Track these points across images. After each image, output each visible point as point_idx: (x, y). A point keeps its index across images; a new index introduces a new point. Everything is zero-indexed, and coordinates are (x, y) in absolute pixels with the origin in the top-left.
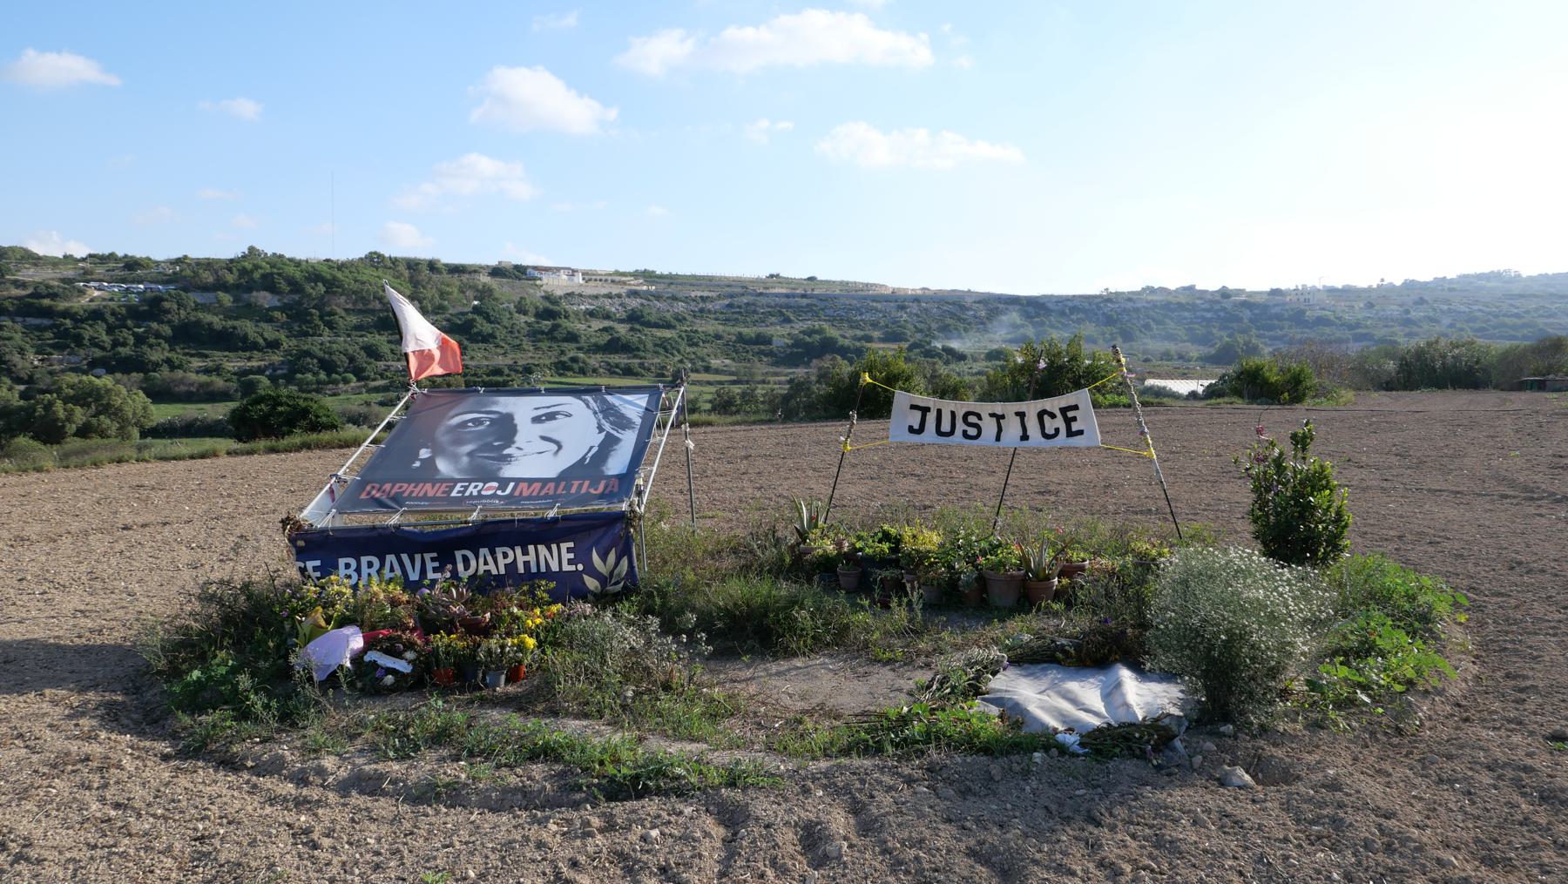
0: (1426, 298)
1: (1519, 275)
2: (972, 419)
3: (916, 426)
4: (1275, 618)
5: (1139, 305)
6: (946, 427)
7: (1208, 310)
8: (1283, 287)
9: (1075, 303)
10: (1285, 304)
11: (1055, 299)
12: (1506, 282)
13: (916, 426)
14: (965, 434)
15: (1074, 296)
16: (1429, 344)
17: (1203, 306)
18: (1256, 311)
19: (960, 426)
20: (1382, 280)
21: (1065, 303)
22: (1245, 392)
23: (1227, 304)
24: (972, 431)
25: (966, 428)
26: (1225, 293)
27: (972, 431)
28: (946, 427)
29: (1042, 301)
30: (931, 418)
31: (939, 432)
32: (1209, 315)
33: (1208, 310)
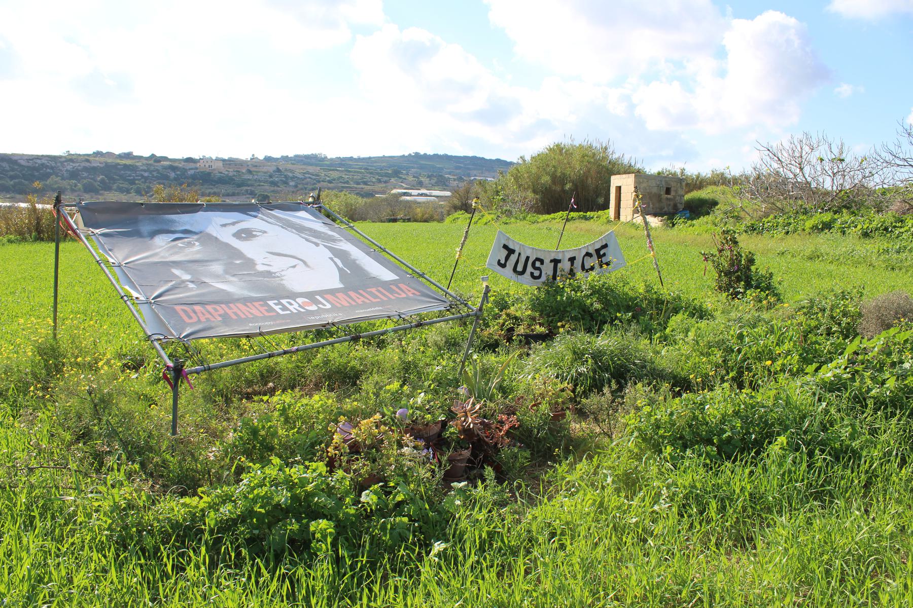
0: (281, 168)
1: (326, 157)
2: (538, 264)
3: (503, 262)
4: (818, 496)
5: (95, 165)
6: (520, 268)
7: (145, 171)
8: (196, 156)
9: (43, 161)
10: (197, 168)
11: (26, 158)
12: (320, 161)
13: (503, 262)
14: (532, 274)
15: (42, 156)
16: (818, 236)
17: (141, 168)
18: (178, 173)
19: (530, 269)
20: (253, 155)
21: (35, 160)
22: (76, 221)
23: (158, 166)
24: (537, 273)
25: (533, 271)
26: (296, 156)
27: (537, 273)
28: (520, 268)
29: (15, 158)
30: (513, 258)
31: (515, 270)
32: (146, 174)
33: (145, 171)
